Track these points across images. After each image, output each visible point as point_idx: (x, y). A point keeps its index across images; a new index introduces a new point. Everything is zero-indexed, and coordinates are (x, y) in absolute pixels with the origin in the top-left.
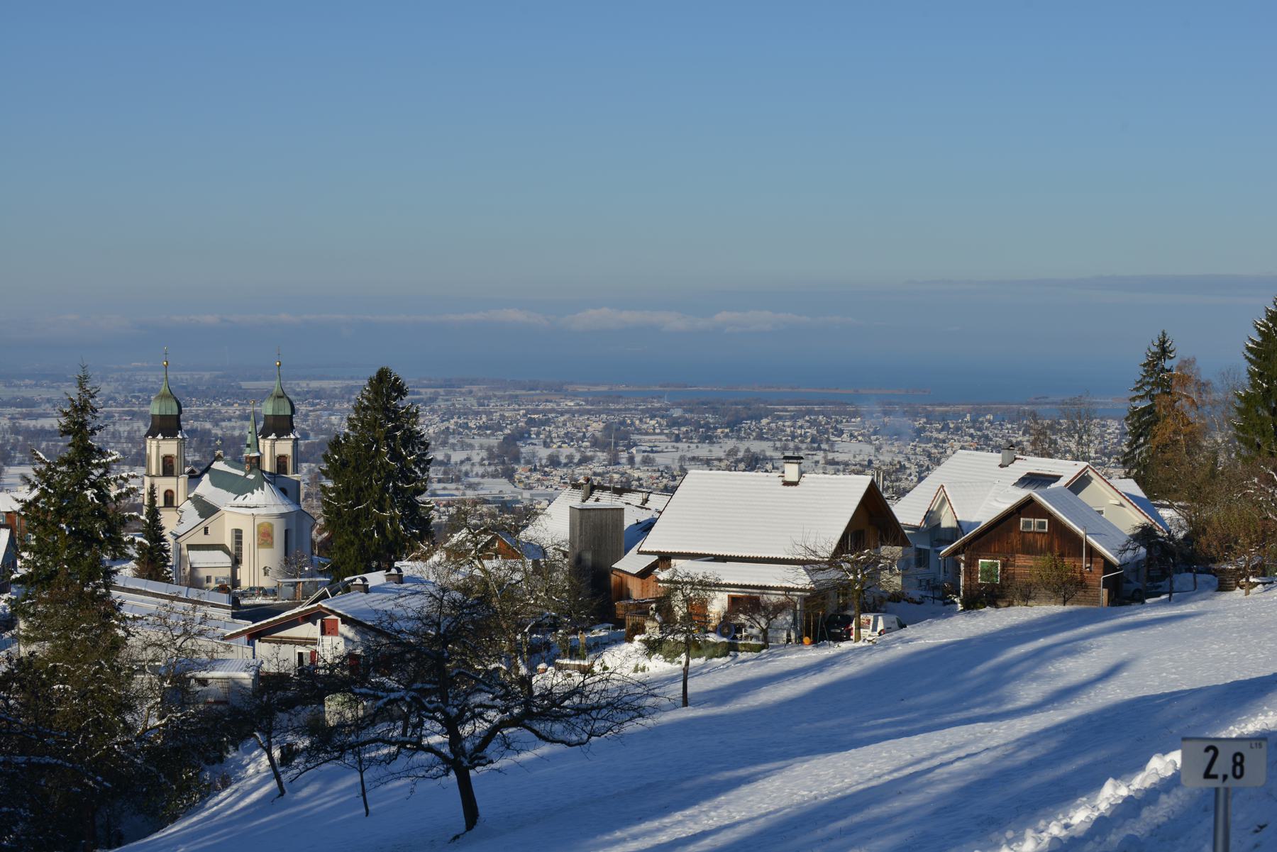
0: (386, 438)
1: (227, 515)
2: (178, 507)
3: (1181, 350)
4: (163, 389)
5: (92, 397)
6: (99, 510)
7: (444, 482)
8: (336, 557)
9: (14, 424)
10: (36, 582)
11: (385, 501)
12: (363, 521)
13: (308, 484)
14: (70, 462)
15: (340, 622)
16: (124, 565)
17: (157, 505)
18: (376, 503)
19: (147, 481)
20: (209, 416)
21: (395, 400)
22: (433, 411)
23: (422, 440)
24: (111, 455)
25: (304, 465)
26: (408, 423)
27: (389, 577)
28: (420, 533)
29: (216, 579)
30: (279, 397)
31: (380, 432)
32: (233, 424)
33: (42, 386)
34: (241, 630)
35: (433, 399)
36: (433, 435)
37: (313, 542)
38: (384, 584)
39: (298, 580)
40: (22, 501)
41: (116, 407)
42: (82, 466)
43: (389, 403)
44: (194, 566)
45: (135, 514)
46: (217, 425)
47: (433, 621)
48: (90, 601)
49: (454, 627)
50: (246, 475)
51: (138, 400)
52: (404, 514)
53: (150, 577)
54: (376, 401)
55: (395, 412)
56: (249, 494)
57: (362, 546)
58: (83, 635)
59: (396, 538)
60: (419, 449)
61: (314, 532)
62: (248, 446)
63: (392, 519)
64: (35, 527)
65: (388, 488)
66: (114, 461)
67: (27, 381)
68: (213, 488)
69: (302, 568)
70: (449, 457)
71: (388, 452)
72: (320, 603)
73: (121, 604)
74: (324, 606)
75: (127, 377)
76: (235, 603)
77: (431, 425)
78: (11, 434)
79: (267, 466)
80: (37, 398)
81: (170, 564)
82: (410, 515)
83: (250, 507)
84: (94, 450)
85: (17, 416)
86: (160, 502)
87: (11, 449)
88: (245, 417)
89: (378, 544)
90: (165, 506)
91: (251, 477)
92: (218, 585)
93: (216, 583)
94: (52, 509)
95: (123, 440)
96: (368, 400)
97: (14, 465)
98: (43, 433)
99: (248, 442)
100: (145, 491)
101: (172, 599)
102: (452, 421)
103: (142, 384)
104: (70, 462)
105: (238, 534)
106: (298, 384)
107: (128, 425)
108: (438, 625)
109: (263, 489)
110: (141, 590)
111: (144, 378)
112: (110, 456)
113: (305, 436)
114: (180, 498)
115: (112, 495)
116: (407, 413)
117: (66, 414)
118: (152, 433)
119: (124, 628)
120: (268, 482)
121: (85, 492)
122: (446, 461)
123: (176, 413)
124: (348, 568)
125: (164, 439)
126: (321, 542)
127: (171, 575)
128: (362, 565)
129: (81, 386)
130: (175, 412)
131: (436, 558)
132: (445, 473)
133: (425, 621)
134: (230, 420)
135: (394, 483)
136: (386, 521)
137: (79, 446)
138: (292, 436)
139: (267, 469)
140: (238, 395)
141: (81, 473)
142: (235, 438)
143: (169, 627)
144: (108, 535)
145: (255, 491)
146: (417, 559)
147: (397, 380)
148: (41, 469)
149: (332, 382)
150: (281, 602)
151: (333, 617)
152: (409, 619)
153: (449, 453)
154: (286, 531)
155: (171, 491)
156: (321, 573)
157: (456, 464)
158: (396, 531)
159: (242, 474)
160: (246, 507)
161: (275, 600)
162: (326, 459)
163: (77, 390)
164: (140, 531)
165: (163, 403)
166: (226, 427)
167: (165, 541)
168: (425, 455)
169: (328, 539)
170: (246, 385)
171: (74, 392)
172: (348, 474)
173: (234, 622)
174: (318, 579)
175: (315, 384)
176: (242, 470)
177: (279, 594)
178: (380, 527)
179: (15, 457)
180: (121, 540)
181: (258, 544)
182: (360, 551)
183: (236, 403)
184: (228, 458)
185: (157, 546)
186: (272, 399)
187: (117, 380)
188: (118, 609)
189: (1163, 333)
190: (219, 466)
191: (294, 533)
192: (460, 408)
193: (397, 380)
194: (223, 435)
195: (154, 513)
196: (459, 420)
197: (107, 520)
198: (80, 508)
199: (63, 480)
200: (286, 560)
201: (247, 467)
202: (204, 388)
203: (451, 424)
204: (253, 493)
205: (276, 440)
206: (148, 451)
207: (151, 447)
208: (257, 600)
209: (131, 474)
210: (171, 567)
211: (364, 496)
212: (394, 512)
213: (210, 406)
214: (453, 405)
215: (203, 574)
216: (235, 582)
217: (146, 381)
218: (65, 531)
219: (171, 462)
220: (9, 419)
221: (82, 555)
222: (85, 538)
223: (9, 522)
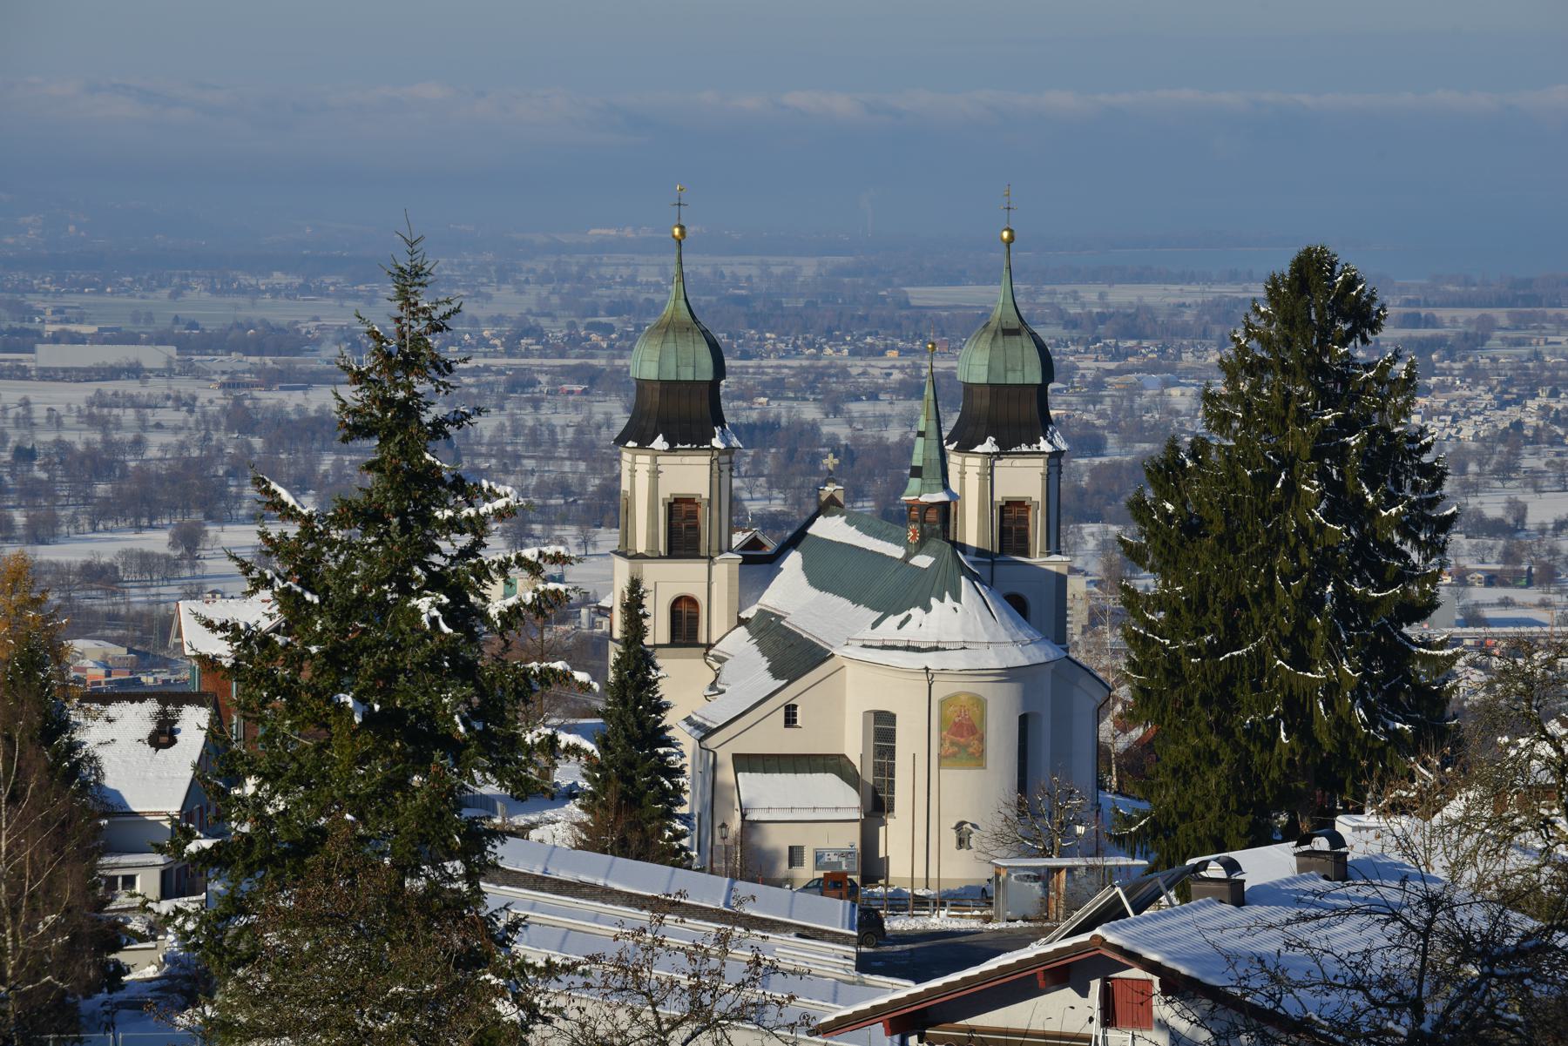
0: (1317, 454)
1: (851, 670)
2: (709, 646)
4: (669, 306)
5: (437, 328)
6: (454, 654)
7: (1504, 584)
8: (1168, 796)
9: (238, 401)
10: (262, 864)
11: (1312, 635)
12: (1245, 695)
13: (1098, 584)
14: (368, 516)
15: (1157, 987)
16: (549, 814)
17: (648, 641)
18: (1287, 641)
19: (622, 571)
20: (813, 383)
21: (1343, 344)
22: (1474, 374)
23: (1427, 458)
24: (491, 495)
25: (1089, 528)
26: (1382, 409)
27: (1307, 860)
28: (1417, 734)
29: (818, 857)
30: (1009, 332)
31: (1298, 438)
32: (882, 407)
33: (322, 292)
34: (866, 1006)
35: (1474, 341)
36: (1474, 446)
37: (1101, 752)
38: (1289, 881)
39: (1055, 862)
40: (223, 627)
41: (543, 355)
42: (405, 528)
43: (1326, 351)
44: (753, 816)
45: (559, 665)
46: (837, 411)
47: (1400, 995)
48: (419, 920)
49: (1467, 1016)
50: (908, 556)
51: (606, 336)
52: (1367, 676)
53: (622, 849)
54: (1289, 344)
55: (1344, 378)
56: (916, 612)
57: (1244, 764)
58: (394, 1018)
59: (1344, 745)
60: (1416, 487)
61: (1107, 727)
62: (917, 472)
63: (1332, 690)
64: (264, 703)
65: (1321, 600)
66: (500, 515)
67: (278, 278)
68: (815, 593)
69: (1066, 828)
70: (1520, 511)
71: (1322, 495)
72: (1098, 931)
73: (514, 926)
74: (1111, 939)
75: (575, 269)
76: (869, 924)
77: (1467, 416)
78: (230, 429)
79: (972, 530)
80: (307, 326)
81: (683, 810)
82: (1386, 679)
83: (918, 650)
84: (442, 481)
85: (247, 377)
86: (658, 629)
87: (228, 474)
88: (911, 390)
89: (1291, 762)
90: (674, 643)
91: (923, 561)
92: (820, 874)
93: (817, 868)
94: (314, 649)
95: (561, 452)
96: (1266, 342)
97: (238, 521)
98: (306, 430)
99: (917, 461)
100: (614, 599)
101: (659, 906)
102: (1532, 405)
103: (617, 290)
104: (368, 516)
105: (883, 727)
106: (1075, 296)
107: (576, 407)
108: (1417, 1007)
109: (957, 597)
110: (594, 887)
111: (625, 272)
112: (488, 499)
113: (1090, 443)
114: (716, 621)
115: (493, 612)
116: (1379, 380)
117: (359, 377)
118: (638, 433)
119: (518, 1000)
120: (973, 577)
121: (414, 602)
122: (1510, 521)
123: (709, 376)
124: (1201, 832)
125: (672, 450)
126: (1128, 751)
127: (685, 842)
128: (1244, 823)
129: (404, 295)
130: (706, 373)
131: (1454, 809)
132: (1508, 556)
133: (1378, 993)
134: (873, 396)
135: (1339, 586)
136: (1312, 698)
137: (397, 469)
138: (1044, 446)
139: (971, 538)
140: (899, 326)
141: (403, 547)
142: (887, 448)
143: (648, 995)
144: (478, 726)
145: (934, 601)
146: (1398, 808)
147: (1351, 283)
148: (283, 535)
149: (1175, 288)
150: (1004, 925)
151: (1136, 973)
152: (1329, 985)
153: (1521, 498)
154: (1023, 720)
155: (692, 601)
156: (1122, 843)
157: (1542, 530)
158: (1343, 725)
159: (897, 552)
160: (908, 648)
161: (988, 919)
162: (1139, 509)
163: (394, 308)
164: (598, 714)
165: (671, 345)
166: (863, 416)
167: (668, 742)
168: (1433, 503)
169: (1145, 745)
170: (921, 295)
171: (383, 313)
172: (1204, 557)
173: (863, 984)
174: (1111, 861)
175: (1123, 296)
176: (897, 542)
177: (1000, 901)
178: (1297, 711)
179: (239, 497)
180: (515, 741)
181: (940, 757)
182: (1236, 779)
183: (893, 347)
184: (867, 506)
185: (646, 758)
186: (987, 337)
187: (545, 279)
188: (504, 943)
189: (422, 237)
190: (829, 528)
191: (1046, 724)
192: (1557, 367)
193: (1351, 283)
194: (854, 439)
195: (638, 662)
196: (1553, 403)
197: (477, 685)
198: (398, 648)
199: (348, 566)
200: (1020, 804)
201: (912, 533)
202: (801, 303)
203: (1530, 415)
204: (927, 608)
205: (998, 456)
206: (625, 485)
207: (633, 471)
208: (934, 920)
209: (550, 550)
210: (686, 819)
211: (1250, 620)
212: (1338, 668)
213: (816, 357)
214: (1537, 356)
215: (777, 840)
216: (872, 865)
217: (631, 281)
218: (351, 713)
219: (693, 515)
220: (223, 386)
221: (402, 783)
222: (412, 736)
223: (209, 687)
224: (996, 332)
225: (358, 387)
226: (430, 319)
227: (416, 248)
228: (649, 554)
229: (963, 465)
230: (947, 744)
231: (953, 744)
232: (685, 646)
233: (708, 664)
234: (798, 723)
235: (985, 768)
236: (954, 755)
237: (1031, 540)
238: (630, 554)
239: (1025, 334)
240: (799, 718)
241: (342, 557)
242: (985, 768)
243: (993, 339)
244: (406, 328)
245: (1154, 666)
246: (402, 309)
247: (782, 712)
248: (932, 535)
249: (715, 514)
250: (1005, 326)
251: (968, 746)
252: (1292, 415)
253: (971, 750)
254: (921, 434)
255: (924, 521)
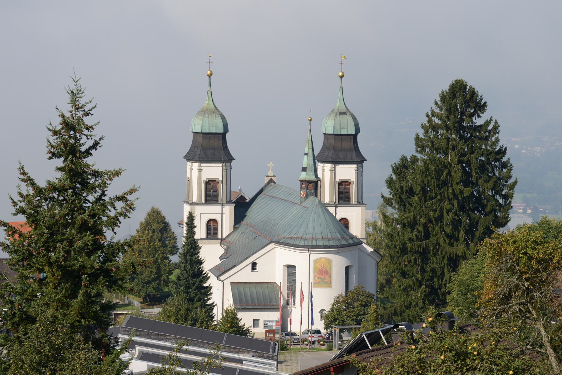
3: (90, 157)
19: (187, 209)
86: (200, 232)
155: (215, 221)
165: (206, 119)
186: (333, 115)
219: (215, 187)
224: (336, 114)
225: (56, 137)
226: (84, 111)
227: (78, 83)
228: (198, 202)
229: (324, 167)
230: (316, 278)
231: (319, 278)
232: (212, 239)
233: (221, 246)
234: (257, 270)
235: (332, 288)
236: (319, 282)
237: (351, 196)
238: (190, 202)
239: (348, 114)
240: (257, 268)
241: (50, 205)
242: (332, 288)
243: (336, 116)
244: (74, 115)
245: (395, 247)
246: (73, 107)
247: (251, 265)
248: (310, 195)
249: (224, 186)
250: (340, 111)
251: (325, 279)
252: (450, 147)
253: (326, 280)
254: (306, 154)
255: (307, 189)
